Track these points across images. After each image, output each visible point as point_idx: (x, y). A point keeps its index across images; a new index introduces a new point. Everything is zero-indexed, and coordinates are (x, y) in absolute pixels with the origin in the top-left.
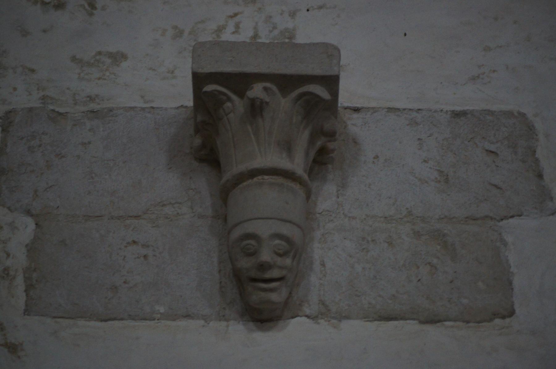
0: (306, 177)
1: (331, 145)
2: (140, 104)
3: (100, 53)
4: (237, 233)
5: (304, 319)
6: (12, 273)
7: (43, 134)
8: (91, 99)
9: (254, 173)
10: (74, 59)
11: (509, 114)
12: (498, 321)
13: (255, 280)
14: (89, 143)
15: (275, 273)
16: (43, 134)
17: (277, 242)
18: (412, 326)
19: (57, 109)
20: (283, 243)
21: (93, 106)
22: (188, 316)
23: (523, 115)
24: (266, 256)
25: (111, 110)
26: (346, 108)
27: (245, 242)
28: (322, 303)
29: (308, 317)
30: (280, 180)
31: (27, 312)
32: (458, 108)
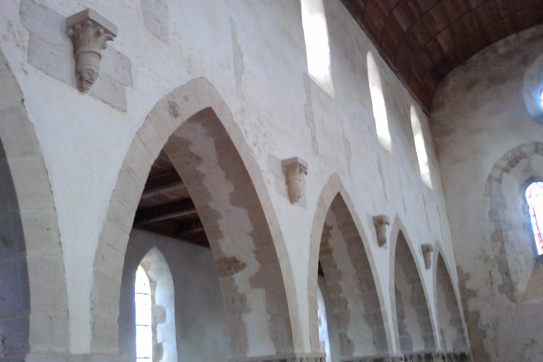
18: (109, 107)
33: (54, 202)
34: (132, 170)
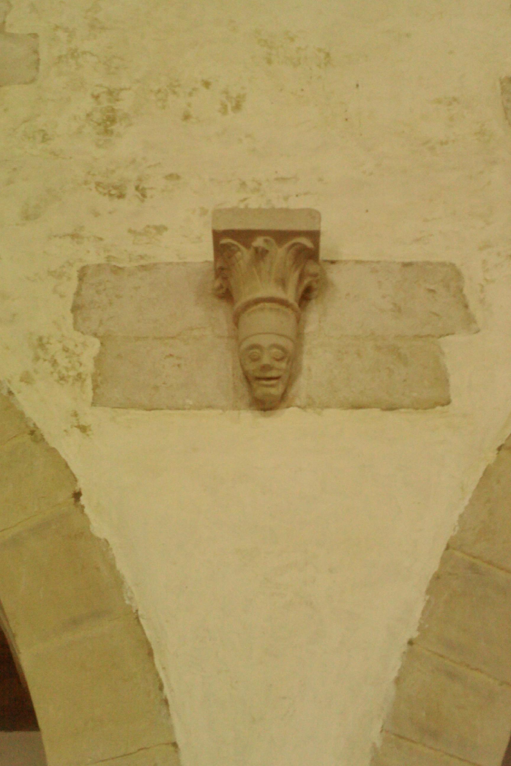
0: (296, 305)
1: (315, 285)
2: (176, 260)
3: (148, 226)
4: (245, 345)
5: (295, 409)
6: (83, 376)
7: (108, 281)
8: (142, 257)
9: (257, 301)
10: (130, 231)
11: (443, 264)
12: (439, 408)
13: (259, 379)
14: (139, 287)
15: (274, 374)
16: (108, 281)
17: (275, 350)
18: (376, 412)
19: (118, 265)
20: (280, 351)
21: (143, 262)
22: (210, 407)
23: (453, 265)
24: (266, 360)
25: (155, 264)
26: (325, 261)
27: (252, 351)
28: (309, 397)
29: (299, 407)
30: (276, 306)
31: (94, 404)
32: (407, 260)
33: (171, 729)
34: (490, 563)
